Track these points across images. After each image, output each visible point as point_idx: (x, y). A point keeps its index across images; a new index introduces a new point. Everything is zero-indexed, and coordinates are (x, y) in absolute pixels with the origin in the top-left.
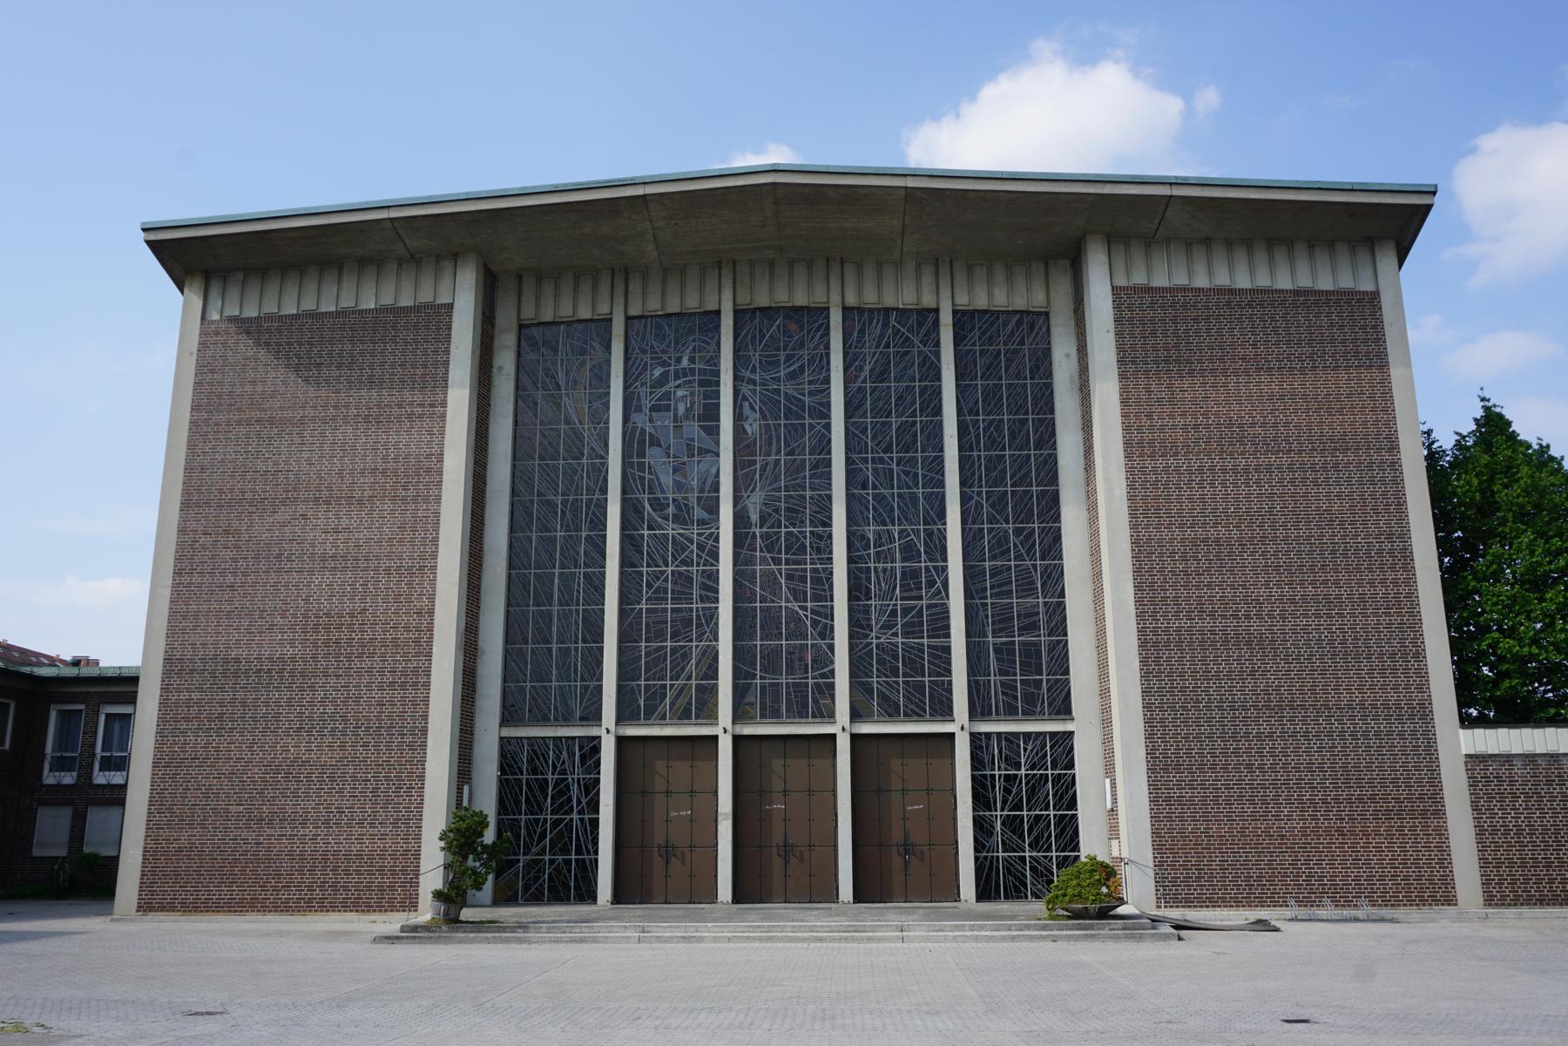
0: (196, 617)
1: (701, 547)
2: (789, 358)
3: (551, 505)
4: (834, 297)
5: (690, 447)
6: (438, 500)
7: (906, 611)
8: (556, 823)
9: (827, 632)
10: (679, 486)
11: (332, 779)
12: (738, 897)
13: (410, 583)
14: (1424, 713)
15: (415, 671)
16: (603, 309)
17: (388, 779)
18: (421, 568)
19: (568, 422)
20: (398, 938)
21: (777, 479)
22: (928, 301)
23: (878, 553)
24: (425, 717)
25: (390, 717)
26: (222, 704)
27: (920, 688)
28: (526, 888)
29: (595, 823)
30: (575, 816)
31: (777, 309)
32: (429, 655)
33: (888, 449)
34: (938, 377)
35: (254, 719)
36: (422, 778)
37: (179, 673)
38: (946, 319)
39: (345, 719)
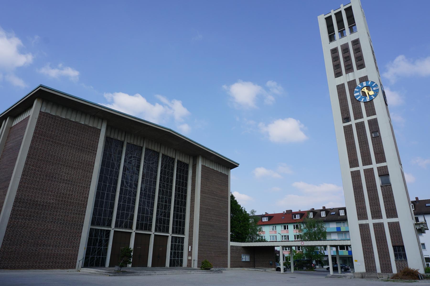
0: (27, 188)
1: (133, 193)
2: (152, 160)
3: (107, 178)
4: (162, 151)
5: (134, 173)
6: (92, 172)
7: (164, 212)
8: (98, 249)
9: (152, 214)
10: (131, 180)
11: (59, 235)
12: (153, 265)
13: (83, 190)
14: (227, 239)
15: (82, 211)
16: (123, 139)
17: (72, 236)
18: (87, 187)
19: (112, 160)
21: (147, 183)
22: (174, 157)
24: (83, 222)
25: (75, 221)
26: (31, 212)
27: (164, 227)
28: (90, 263)
29: (107, 249)
30: (103, 247)
31: (151, 150)
32: (86, 208)
33: (165, 182)
35: (40, 217)
36: (80, 237)
37: (19, 202)
38: (176, 161)
39: (64, 220)
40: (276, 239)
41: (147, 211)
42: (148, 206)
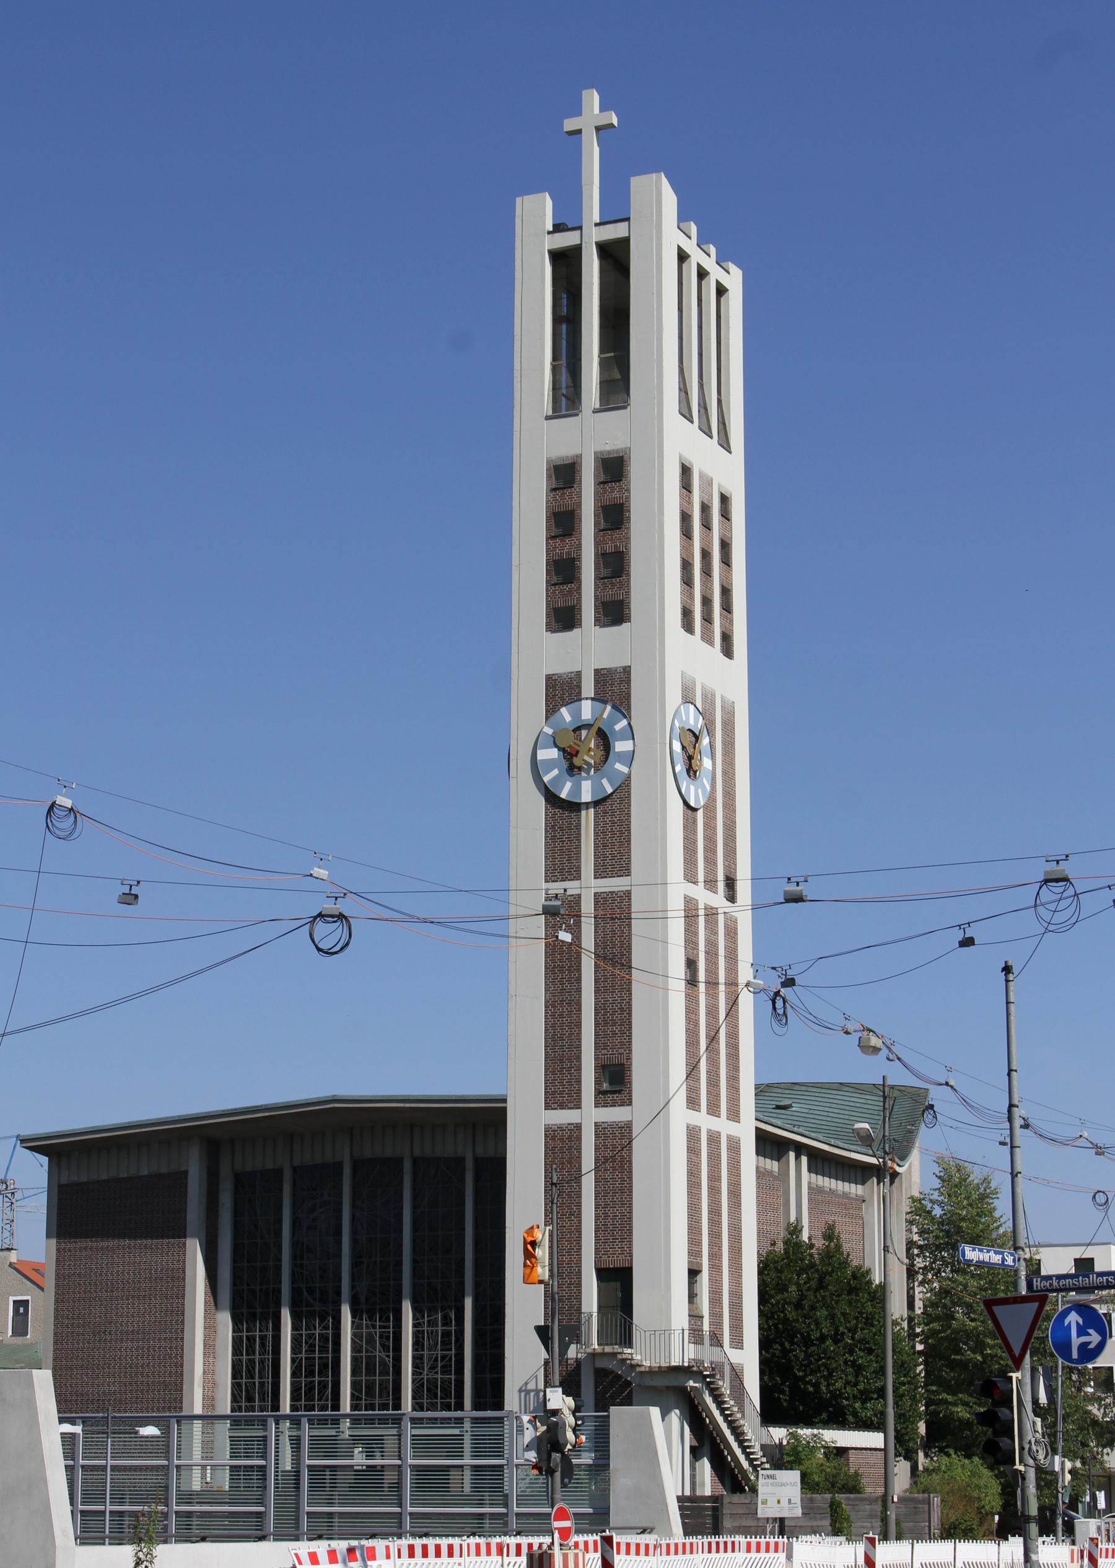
7: (443, 1358)
20: (899, 1059)
23: (429, 1321)
34: (464, 1205)
40: (880, 1450)
41: (383, 1364)
42: (385, 1348)
